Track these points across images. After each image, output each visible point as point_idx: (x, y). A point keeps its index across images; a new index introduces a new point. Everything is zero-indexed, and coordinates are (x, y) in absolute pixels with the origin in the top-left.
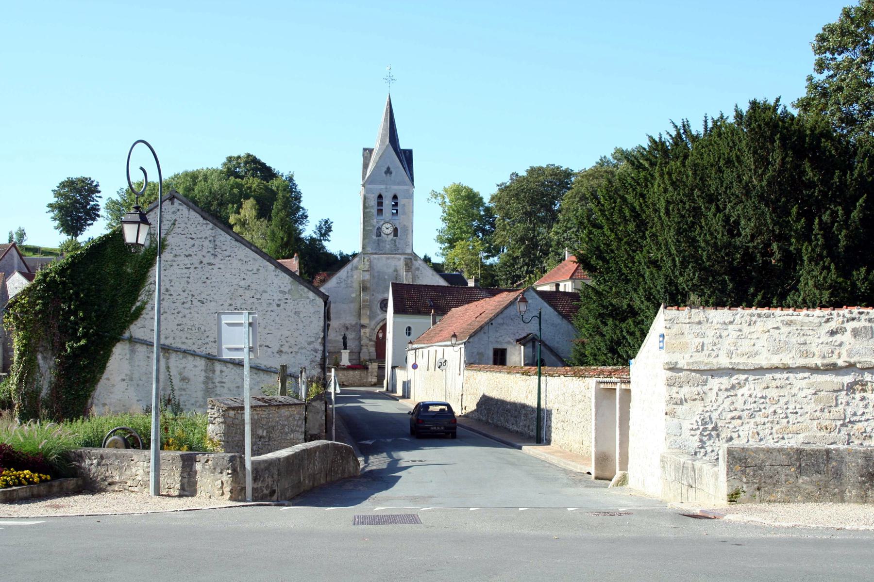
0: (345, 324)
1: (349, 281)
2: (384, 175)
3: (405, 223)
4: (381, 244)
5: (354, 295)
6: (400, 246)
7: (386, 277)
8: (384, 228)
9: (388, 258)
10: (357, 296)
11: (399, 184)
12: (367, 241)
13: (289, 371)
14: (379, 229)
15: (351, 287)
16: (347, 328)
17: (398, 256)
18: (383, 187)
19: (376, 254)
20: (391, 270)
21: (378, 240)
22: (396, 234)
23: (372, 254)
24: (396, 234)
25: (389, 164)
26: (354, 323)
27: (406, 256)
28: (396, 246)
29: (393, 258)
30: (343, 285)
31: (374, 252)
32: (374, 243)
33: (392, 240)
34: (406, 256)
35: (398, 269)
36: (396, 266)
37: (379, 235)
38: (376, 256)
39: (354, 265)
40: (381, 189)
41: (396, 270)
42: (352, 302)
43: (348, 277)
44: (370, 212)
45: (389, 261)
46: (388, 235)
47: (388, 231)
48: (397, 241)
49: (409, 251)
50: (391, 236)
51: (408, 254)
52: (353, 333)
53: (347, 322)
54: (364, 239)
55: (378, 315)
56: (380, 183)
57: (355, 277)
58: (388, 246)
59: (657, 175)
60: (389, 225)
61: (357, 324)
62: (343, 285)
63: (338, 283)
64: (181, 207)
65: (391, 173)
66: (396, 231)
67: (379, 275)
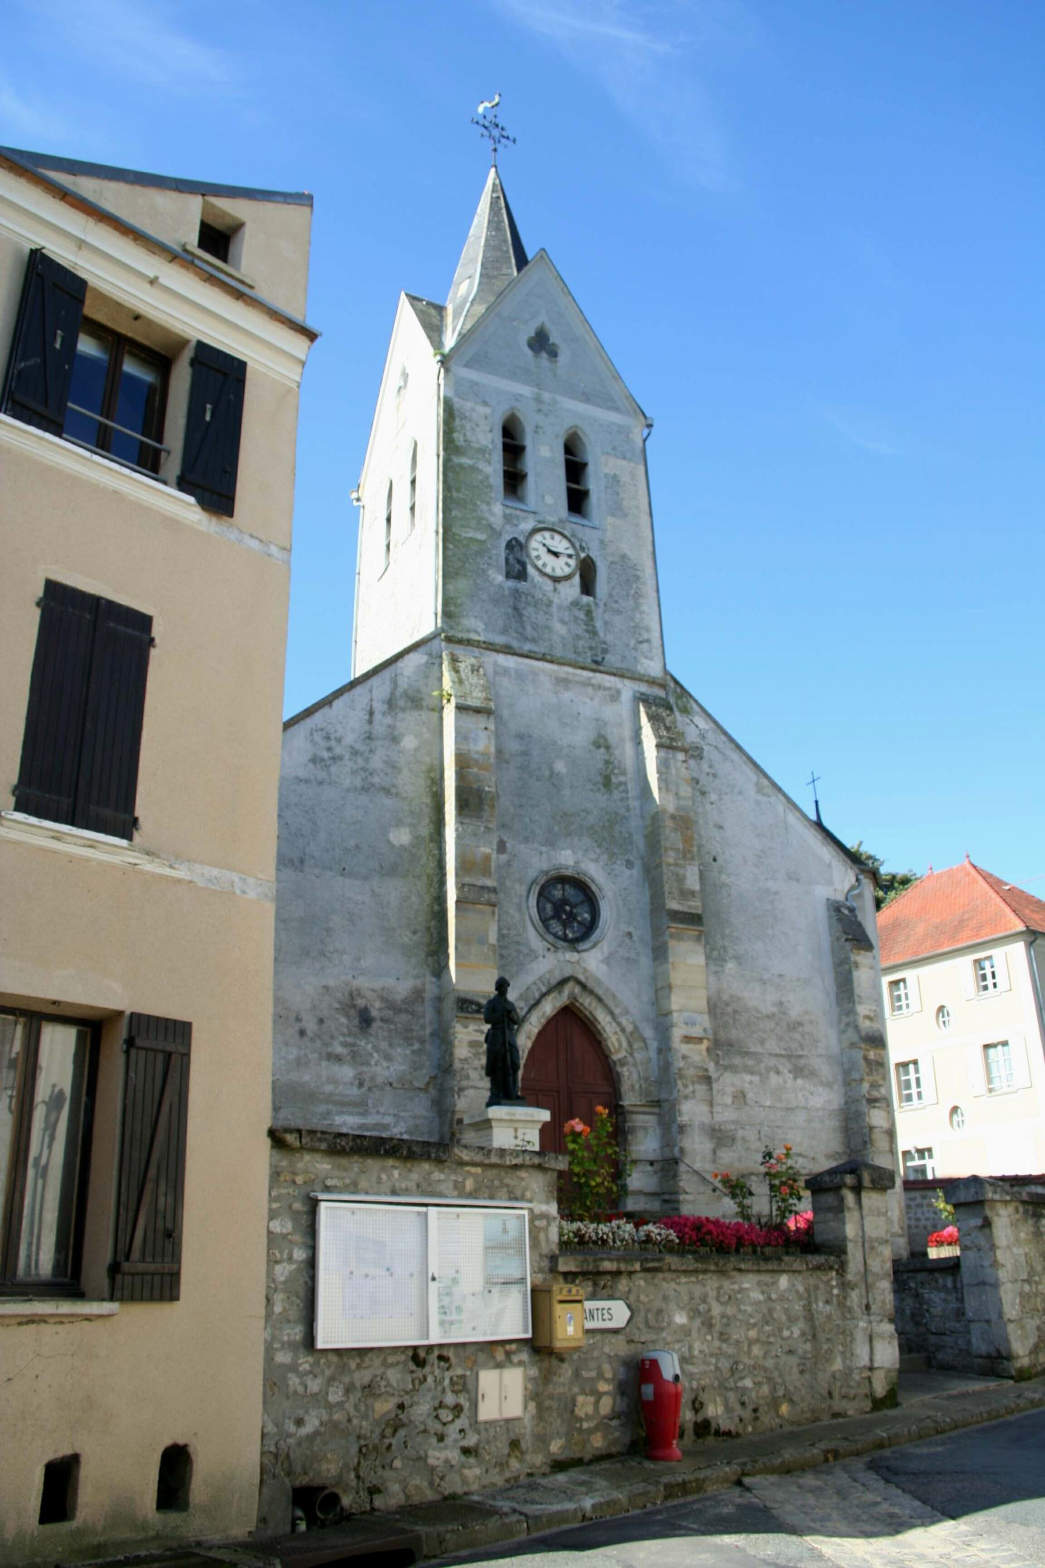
0: (353, 995)
1: (376, 762)
2: (529, 353)
3: (625, 548)
4: (529, 612)
5: (401, 837)
6: (610, 638)
7: (560, 767)
8: (536, 546)
9: (564, 682)
10: (417, 839)
11: (586, 398)
12: (462, 584)
13: (311, 1376)
14: (516, 547)
15: (387, 791)
16: (365, 1020)
17: (608, 681)
18: (526, 390)
19: (508, 650)
20: (580, 738)
21: (516, 594)
22: (588, 587)
23: (490, 647)
24: (588, 587)
25: (543, 318)
26: (402, 989)
27: (643, 688)
28: (594, 633)
29: (587, 684)
30: (344, 774)
31: (500, 640)
32: (496, 601)
33: (575, 604)
34: (643, 688)
35: (613, 740)
36: (600, 723)
37: (517, 570)
38: (510, 662)
39: (403, 683)
40: (518, 398)
41: (601, 743)
42: (391, 871)
43: (369, 737)
44: (473, 469)
45: (567, 696)
46: (556, 580)
47: (561, 566)
48: (598, 613)
49: (652, 668)
50: (572, 590)
51: (652, 682)
52: (400, 1052)
53: (363, 983)
54: (449, 573)
55: (533, 955)
56: (513, 375)
57: (409, 743)
58: (559, 628)
59: (956, 1540)
60: (560, 544)
61: (418, 995)
62: (344, 774)
63: (315, 760)
64: (514, 1142)
65: (553, 354)
66: (587, 573)
67: (525, 753)
